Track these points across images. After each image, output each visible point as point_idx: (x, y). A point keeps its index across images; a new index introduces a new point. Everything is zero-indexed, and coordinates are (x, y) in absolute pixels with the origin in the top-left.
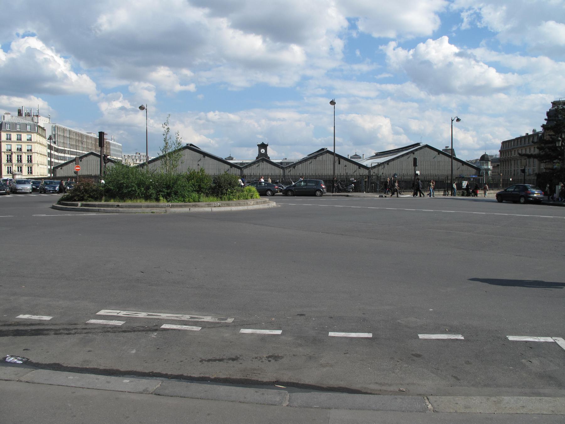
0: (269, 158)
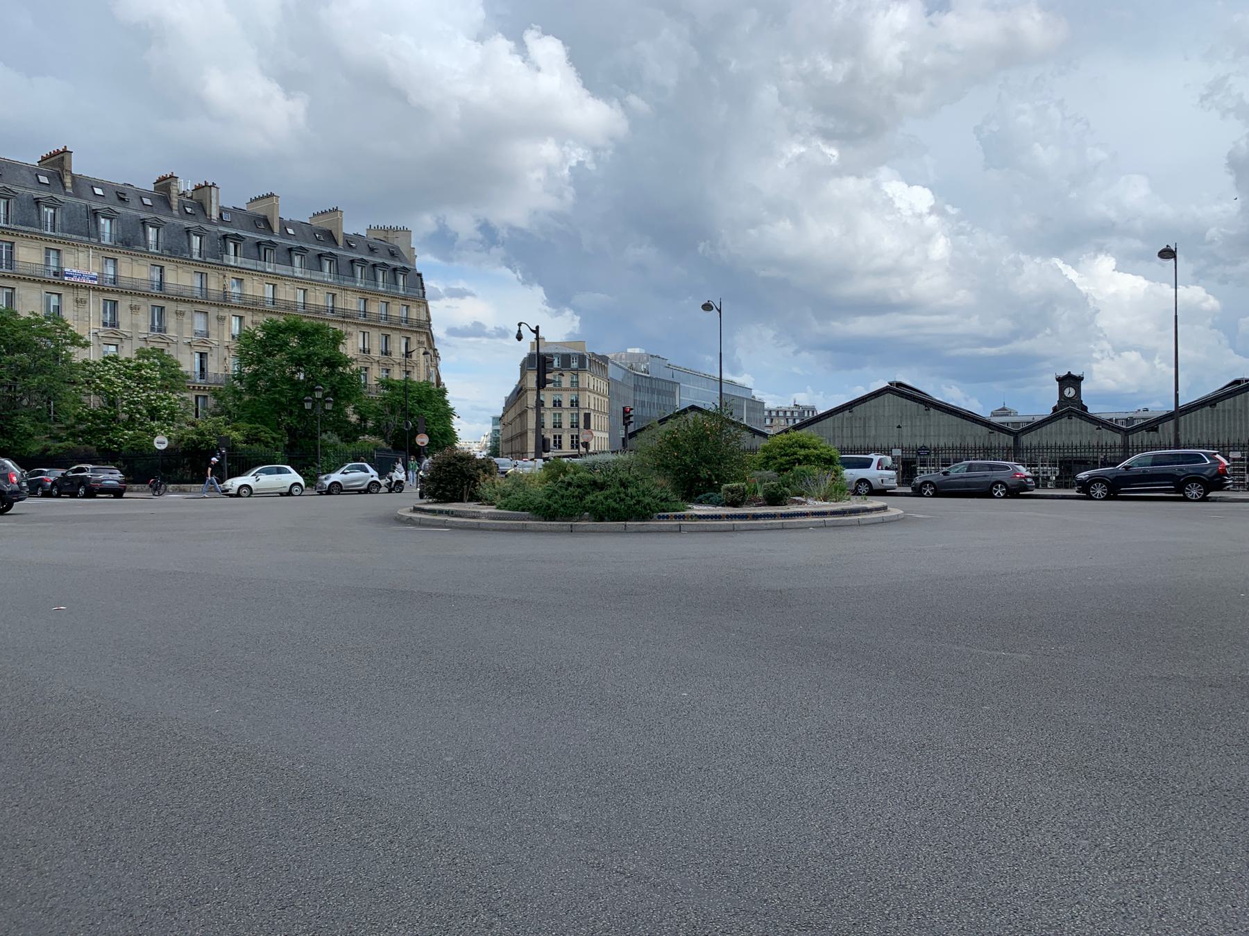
0: (1085, 408)
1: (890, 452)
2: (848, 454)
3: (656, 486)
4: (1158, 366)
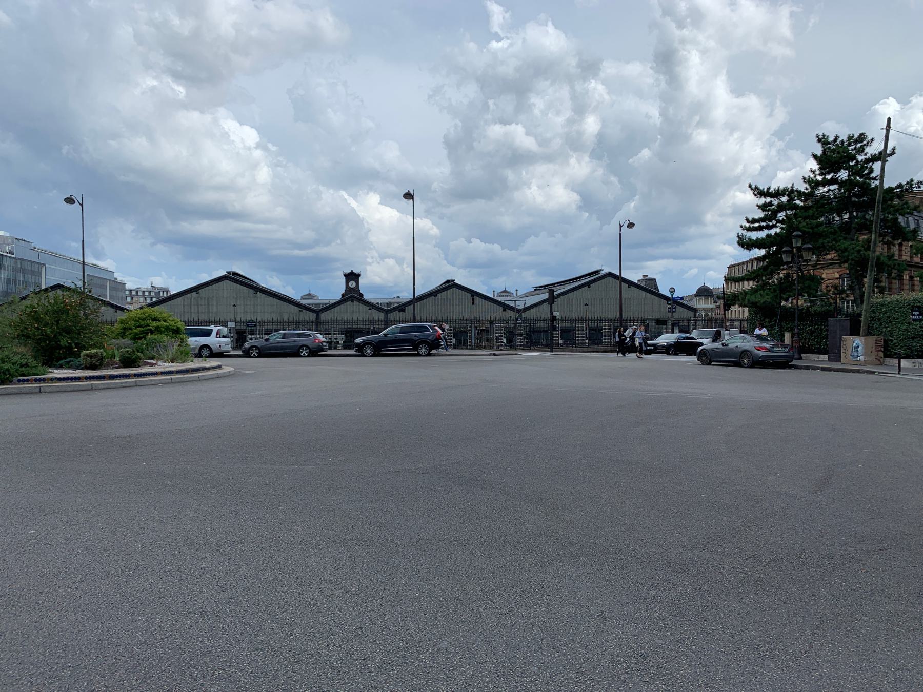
0: (362, 295)
1: (226, 324)
2: (194, 326)
3: (16, 353)
4: (406, 270)
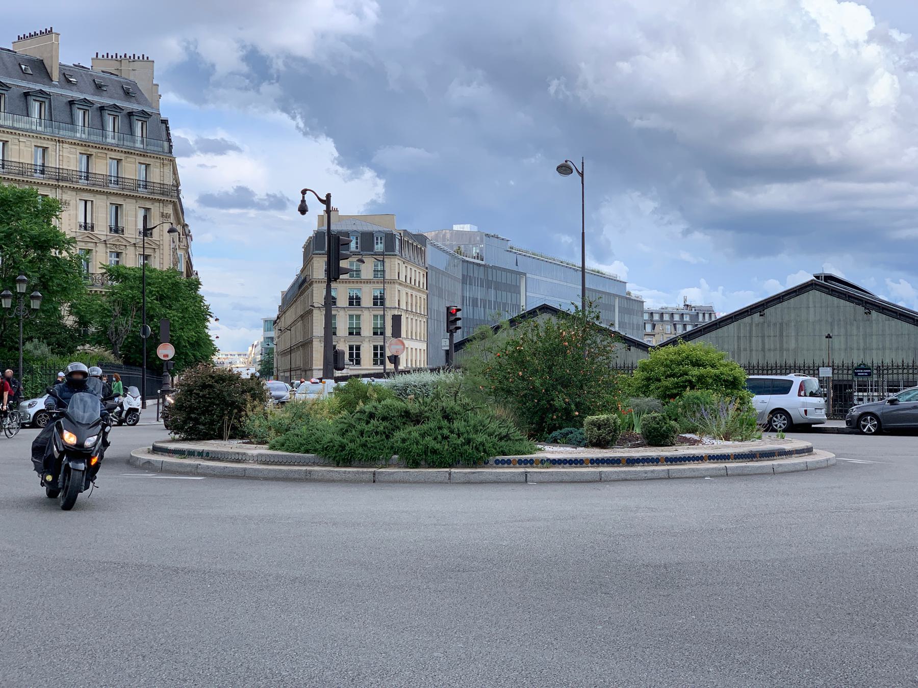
1: (816, 372)
3: (492, 418)
